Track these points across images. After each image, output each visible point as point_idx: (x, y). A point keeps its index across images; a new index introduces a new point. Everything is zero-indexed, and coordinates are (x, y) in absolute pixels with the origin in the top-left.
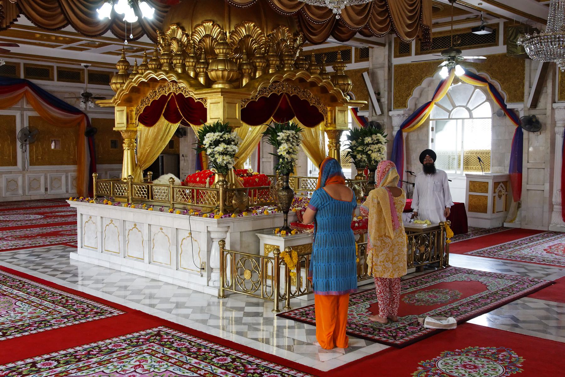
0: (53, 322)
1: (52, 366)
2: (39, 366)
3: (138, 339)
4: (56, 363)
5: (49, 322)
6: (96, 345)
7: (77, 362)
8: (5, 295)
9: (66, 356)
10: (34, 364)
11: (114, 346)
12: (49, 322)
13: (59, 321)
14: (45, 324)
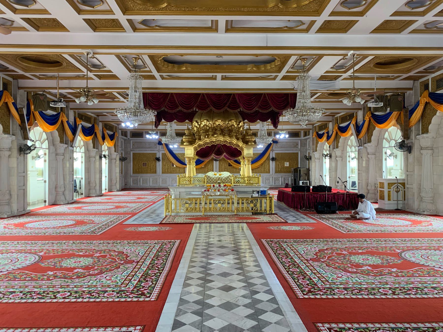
1: (382, 289)
2: (390, 292)
4: (380, 290)
7: (367, 288)
8: (306, 260)
10: (394, 293)
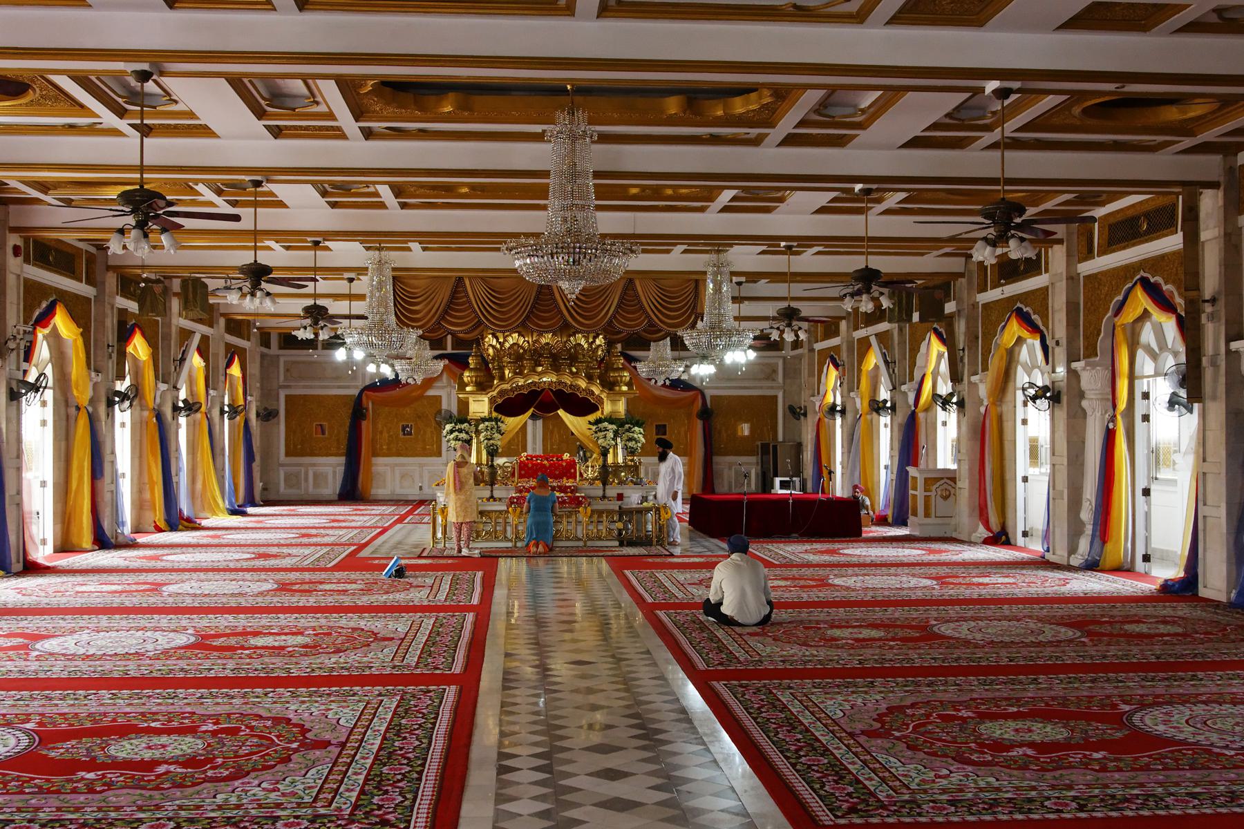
0: (1170, 800)
3: (1144, 806)
5: (919, 806)
6: (1219, 810)
9: (1030, 811)
11: (1188, 802)
12: (919, 806)
13: (1183, 801)
14: (911, 809)
